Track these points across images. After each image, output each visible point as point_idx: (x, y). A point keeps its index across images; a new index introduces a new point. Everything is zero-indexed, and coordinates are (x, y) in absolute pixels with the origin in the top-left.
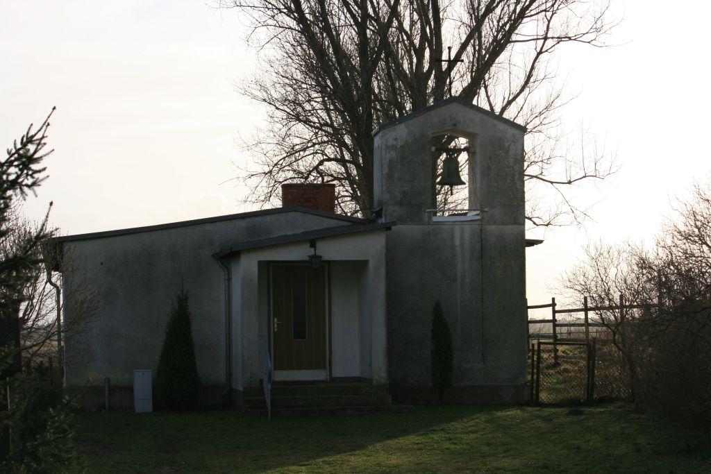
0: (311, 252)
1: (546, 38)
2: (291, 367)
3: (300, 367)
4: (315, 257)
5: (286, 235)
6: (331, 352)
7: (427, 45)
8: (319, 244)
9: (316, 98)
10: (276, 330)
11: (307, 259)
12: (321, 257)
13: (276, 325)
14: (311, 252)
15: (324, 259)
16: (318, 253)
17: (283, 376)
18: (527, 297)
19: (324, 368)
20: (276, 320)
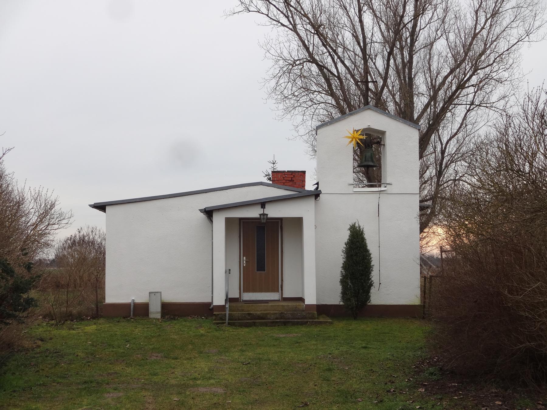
0: (261, 211)
1: (371, 43)
2: (254, 291)
3: (261, 291)
4: (264, 214)
5: (428, 143)
6: (282, 280)
7: (362, 47)
8: (267, 206)
9: (395, 61)
10: (245, 265)
11: (258, 216)
12: (267, 215)
13: (245, 262)
14: (261, 211)
15: (269, 216)
16: (265, 212)
17: (248, 296)
18: (369, 248)
19: (278, 291)
20: (245, 258)
